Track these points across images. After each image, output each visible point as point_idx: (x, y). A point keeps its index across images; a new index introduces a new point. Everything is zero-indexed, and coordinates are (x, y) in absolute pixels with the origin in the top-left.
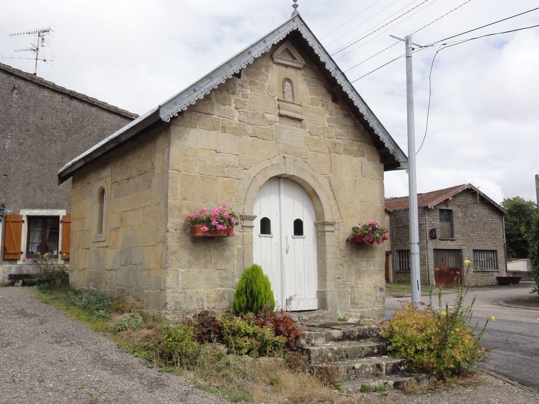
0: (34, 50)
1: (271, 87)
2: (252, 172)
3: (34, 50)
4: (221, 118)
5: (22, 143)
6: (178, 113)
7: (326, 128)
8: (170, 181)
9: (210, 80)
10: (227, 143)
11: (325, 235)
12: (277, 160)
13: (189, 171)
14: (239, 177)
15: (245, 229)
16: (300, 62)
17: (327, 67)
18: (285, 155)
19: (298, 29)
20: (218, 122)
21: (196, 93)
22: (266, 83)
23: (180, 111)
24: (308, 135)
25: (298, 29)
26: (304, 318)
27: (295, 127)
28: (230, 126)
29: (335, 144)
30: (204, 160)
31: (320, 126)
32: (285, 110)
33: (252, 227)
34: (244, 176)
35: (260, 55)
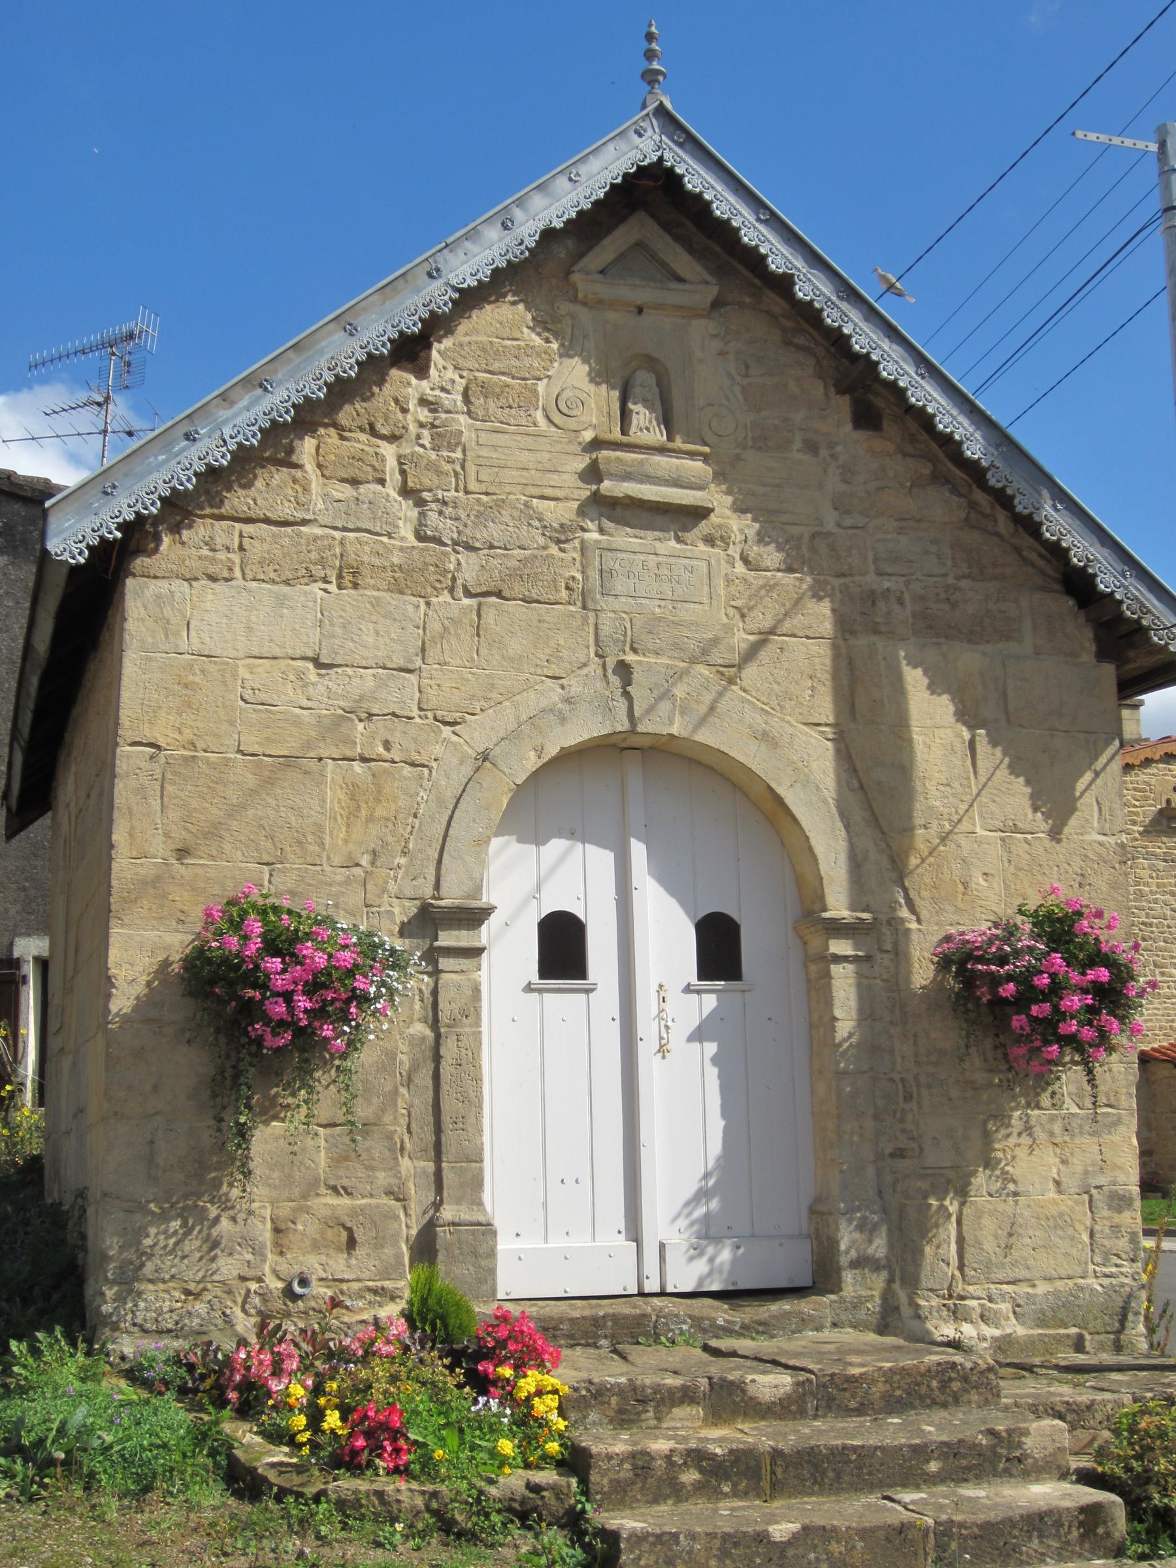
0: (99, 404)
1: (564, 396)
2: (479, 734)
3: (99, 404)
4: (338, 535)
5: (438, 798)
6: (120, 527)
7: (829, 534)
8: (119, 785)
9: (260, 391)
10: (303, 614)
11: (828, 975)
12: (590, 683)
13: (200, 744)
14: (415, 757)
15: (444, 963)
16: (700, 285)
17: (802, 292)
18: (630, 658)
19: (661, 159)
20: (330, 547)
21: (199, 444)
22: (541, 386)
23: (132, 517)
24: (740, 568)
25: (661, 159)
26: (720, 1322)
27: (673, 543)
28: (376, 561)
29: (872, 597)
30: (262, 697)
31: (796, 530)
32: (627, 477)
33: (476, 952)
34: (438, 750)
35: (485, 274)
